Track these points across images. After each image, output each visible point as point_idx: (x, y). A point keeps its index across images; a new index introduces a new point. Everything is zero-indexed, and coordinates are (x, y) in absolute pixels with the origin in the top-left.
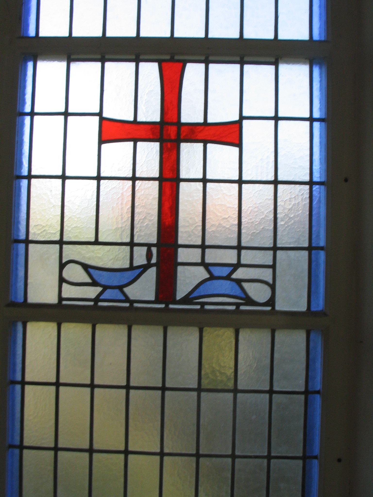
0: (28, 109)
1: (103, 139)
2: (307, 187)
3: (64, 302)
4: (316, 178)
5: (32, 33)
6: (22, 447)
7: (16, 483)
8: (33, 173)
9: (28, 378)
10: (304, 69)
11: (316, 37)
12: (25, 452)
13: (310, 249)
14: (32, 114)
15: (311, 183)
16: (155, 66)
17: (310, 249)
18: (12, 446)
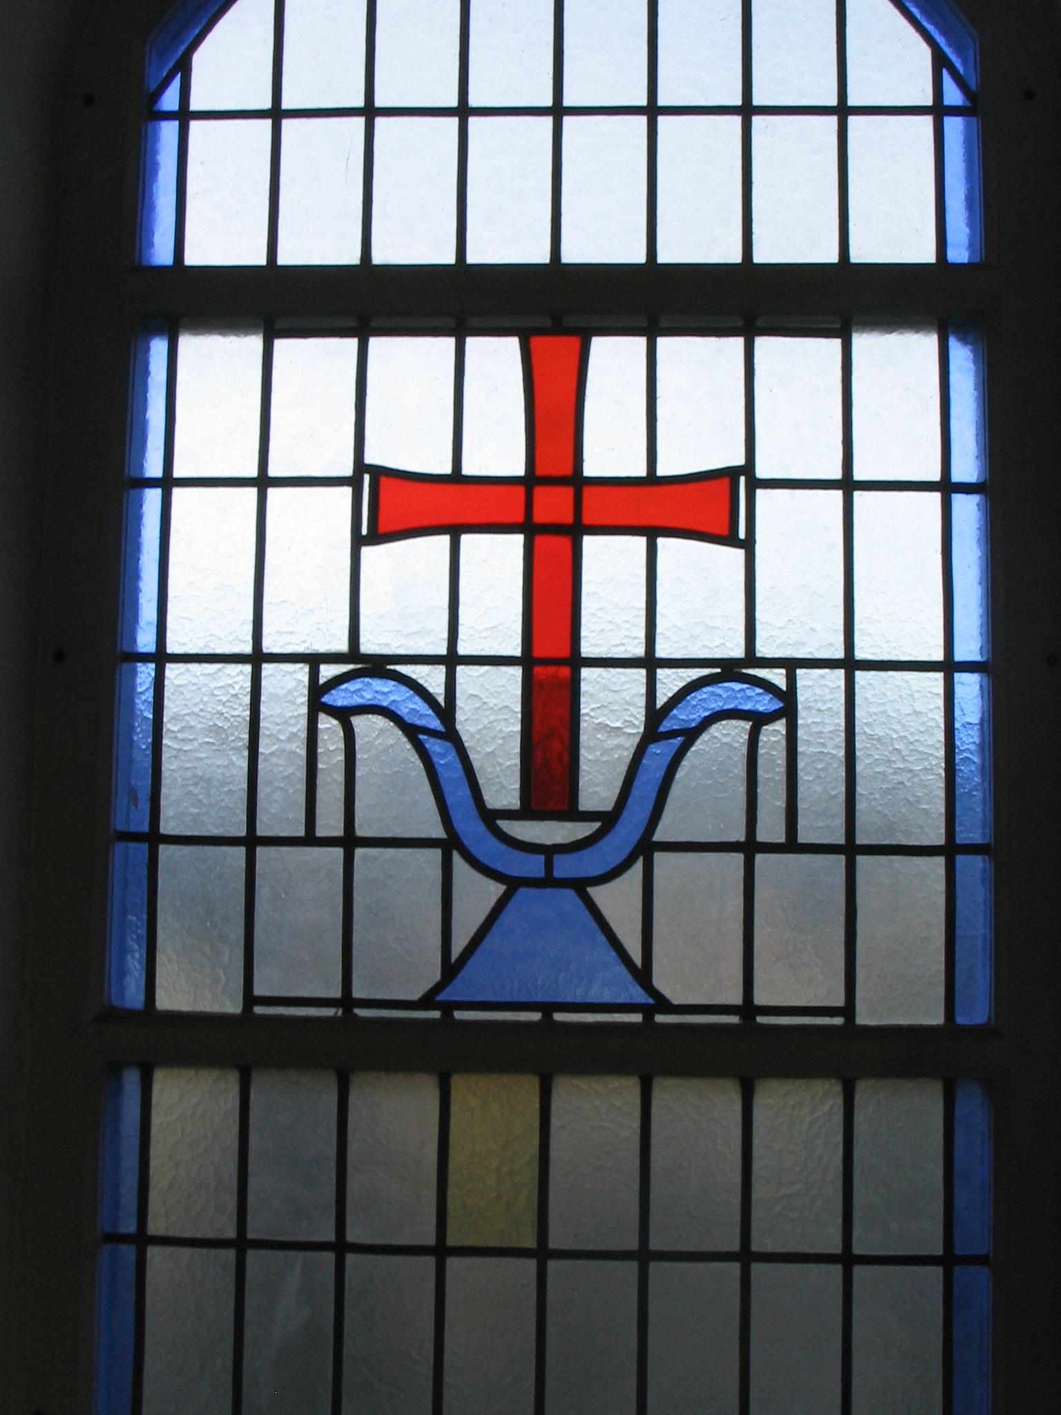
0: (154, 468)
3: (259, 1010)
5: (162, 254)
6: (154, 838)
7: (129, 1297)
8: (178, 473)
10: (924, 345)
11: (959, 254)
12: (165, 851)
13: (948, 1260)
14: (168, 482)
16: (511, 344)
17: (948, 1260)
18: (117, 1238)
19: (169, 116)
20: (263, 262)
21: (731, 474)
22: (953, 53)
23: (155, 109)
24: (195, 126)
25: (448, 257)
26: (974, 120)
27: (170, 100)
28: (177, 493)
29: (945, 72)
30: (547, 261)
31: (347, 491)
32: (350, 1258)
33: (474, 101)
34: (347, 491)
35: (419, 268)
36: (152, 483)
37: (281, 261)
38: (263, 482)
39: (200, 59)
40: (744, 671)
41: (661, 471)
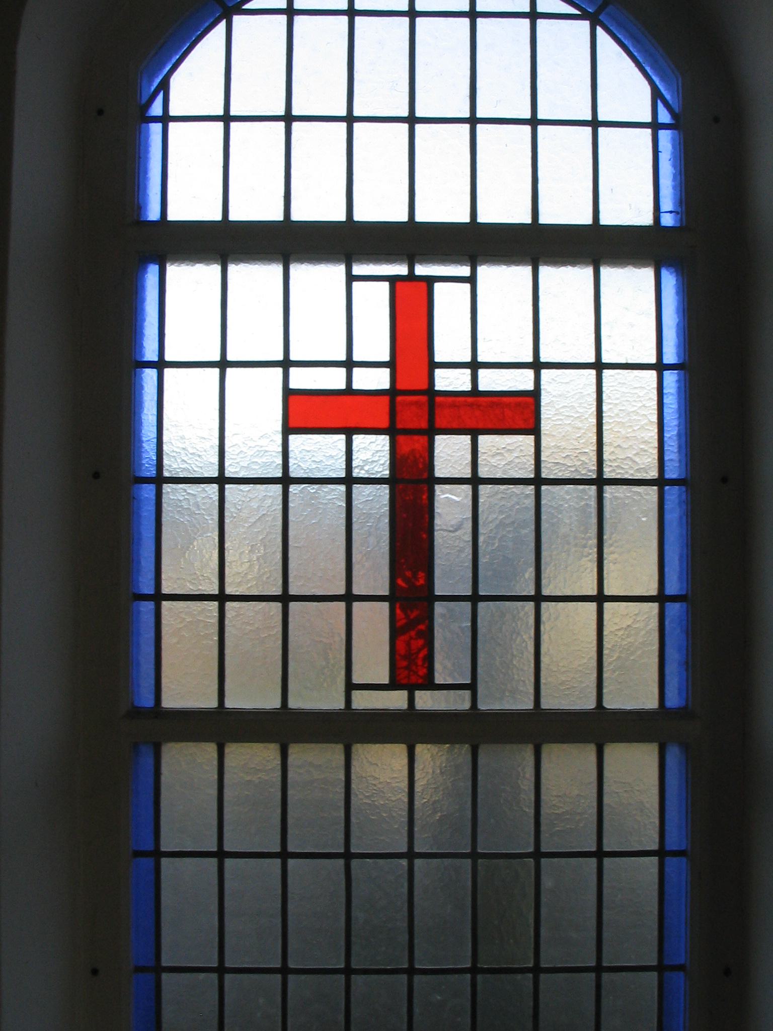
1: (292, 424)
2: (655, 606)
4: (673, 843)
5: (153, 214)
9: (167, 588)
10: (646, 275)
11: (667, 220)
15: (660, 482)
19: (156, 119)
20: (468, 220)
22: (157, 77)
23: (147, 115)
25: (340, 216)
26: (676, 132)
27: (156, 109)
28: (168, 372)
29: (659, 102)
30: (281, 219)
32: (291, 862)
33: (357, 113)
35: (209, 223)
36: (150, 365)
38: (223, 364)
39: (176, 81)
41: (387, 358)
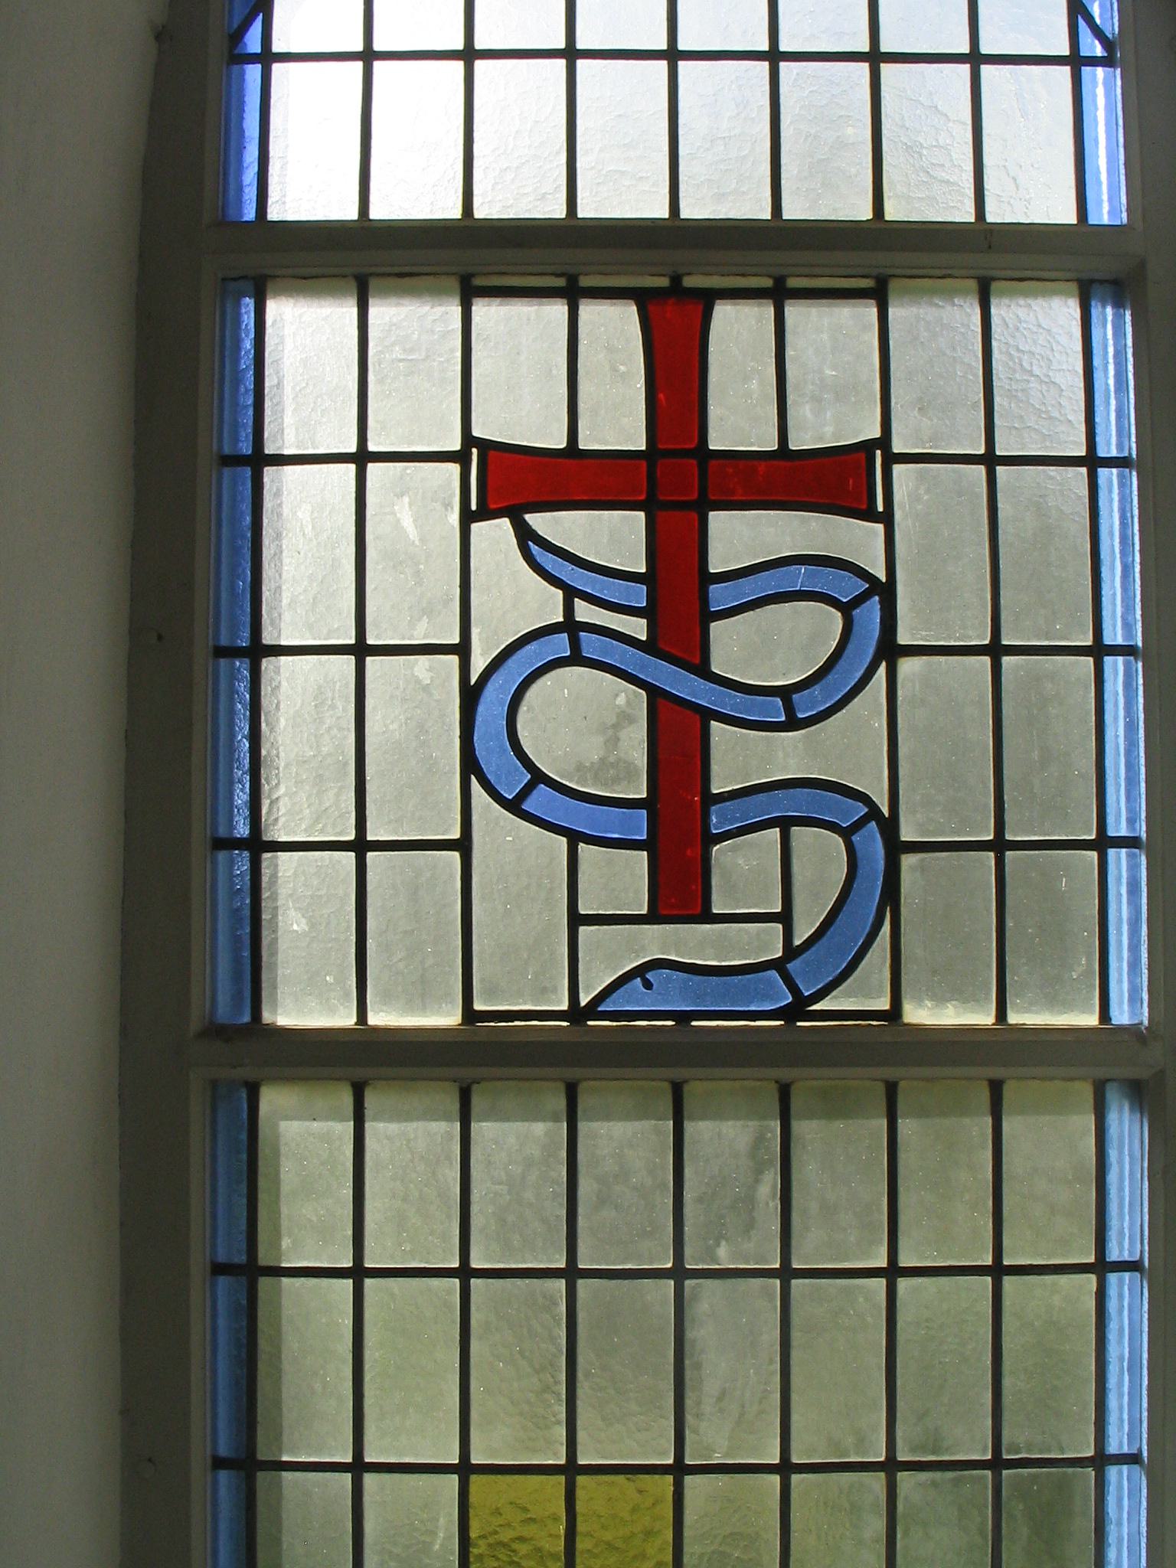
21: (866, 448)
24: (277, 68)
25: (349, 212)
27: (253, 42)
31: (454, 469)
34: (454, 469)
37: (479, 214)
40: (888, 908)
